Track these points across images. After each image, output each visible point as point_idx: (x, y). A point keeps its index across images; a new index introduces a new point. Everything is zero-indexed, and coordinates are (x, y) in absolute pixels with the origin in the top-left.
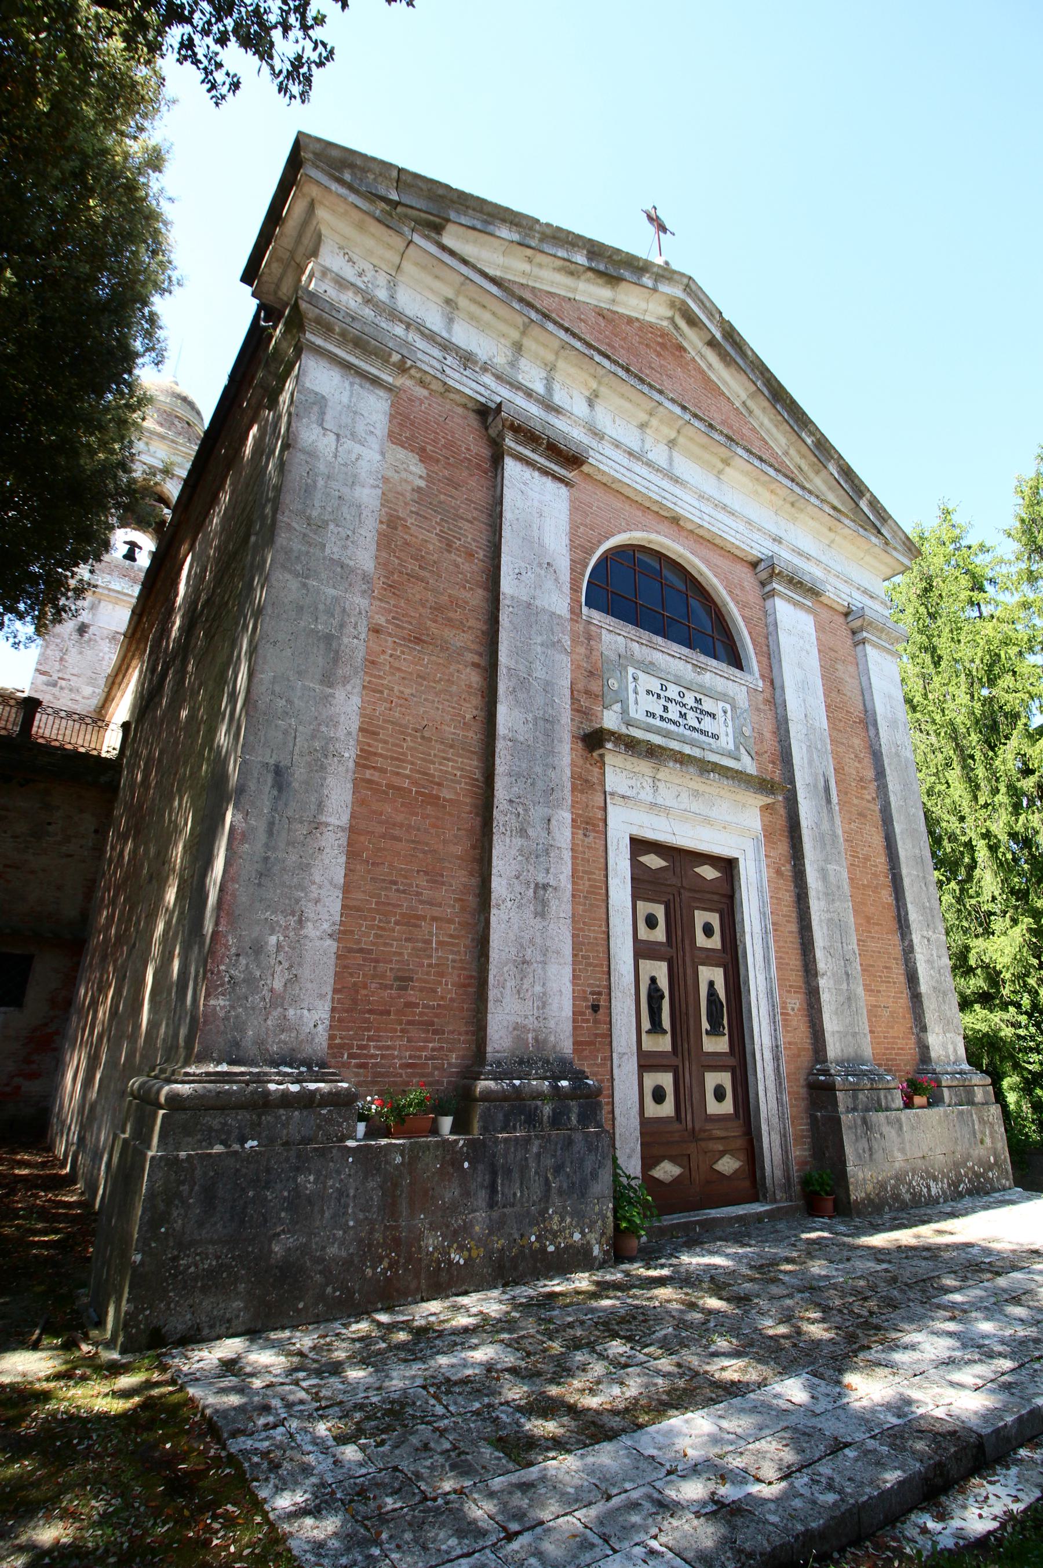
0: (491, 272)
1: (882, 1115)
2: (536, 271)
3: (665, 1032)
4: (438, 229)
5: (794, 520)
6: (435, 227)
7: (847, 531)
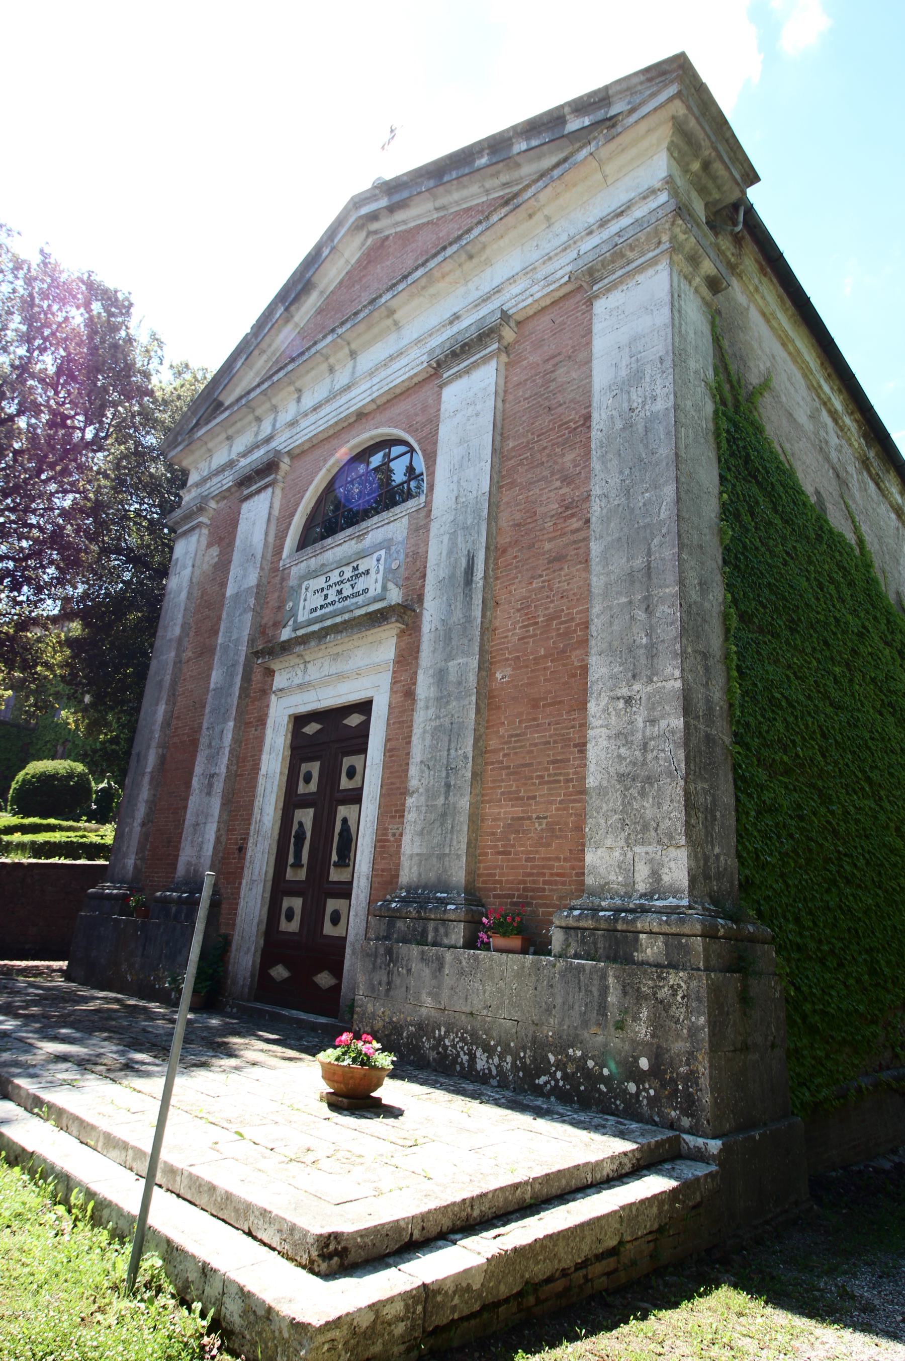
0: (255, 383)
1: (415, 950)
2: (269, 352)
3: (302, 866)
4: (220, 404)
5: (488, 262)
6: (218, 407)
7: (543, 197)
